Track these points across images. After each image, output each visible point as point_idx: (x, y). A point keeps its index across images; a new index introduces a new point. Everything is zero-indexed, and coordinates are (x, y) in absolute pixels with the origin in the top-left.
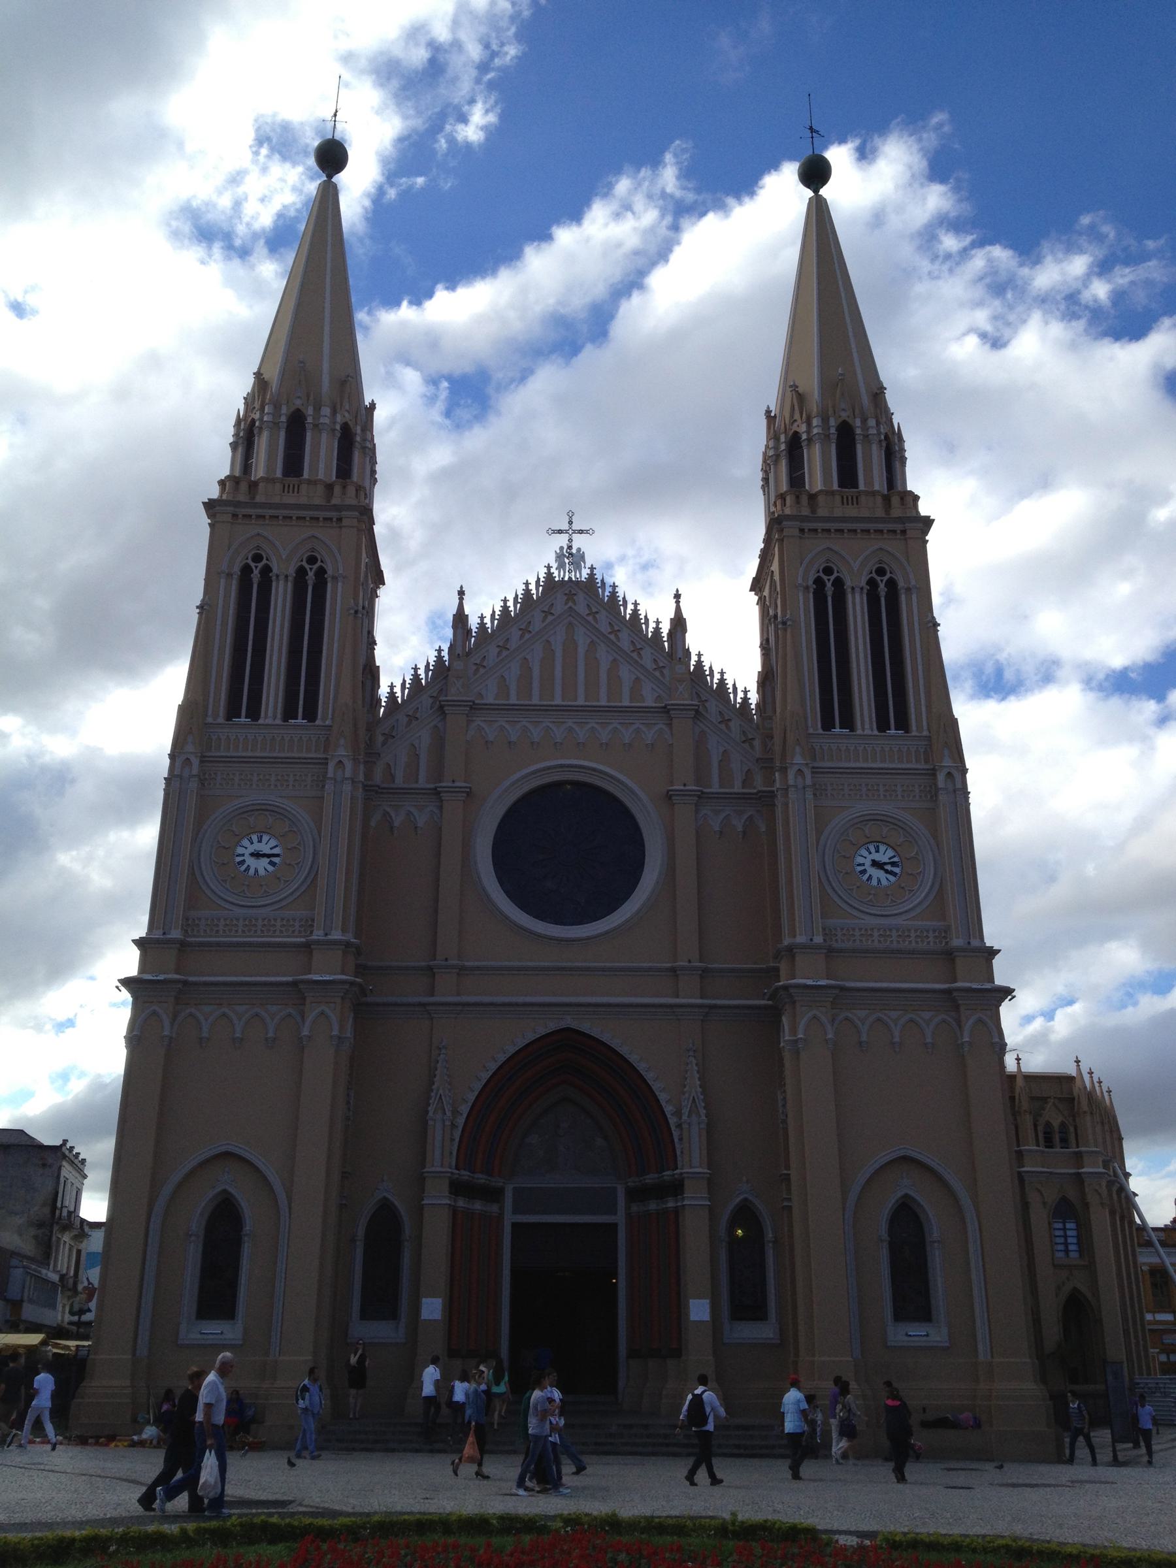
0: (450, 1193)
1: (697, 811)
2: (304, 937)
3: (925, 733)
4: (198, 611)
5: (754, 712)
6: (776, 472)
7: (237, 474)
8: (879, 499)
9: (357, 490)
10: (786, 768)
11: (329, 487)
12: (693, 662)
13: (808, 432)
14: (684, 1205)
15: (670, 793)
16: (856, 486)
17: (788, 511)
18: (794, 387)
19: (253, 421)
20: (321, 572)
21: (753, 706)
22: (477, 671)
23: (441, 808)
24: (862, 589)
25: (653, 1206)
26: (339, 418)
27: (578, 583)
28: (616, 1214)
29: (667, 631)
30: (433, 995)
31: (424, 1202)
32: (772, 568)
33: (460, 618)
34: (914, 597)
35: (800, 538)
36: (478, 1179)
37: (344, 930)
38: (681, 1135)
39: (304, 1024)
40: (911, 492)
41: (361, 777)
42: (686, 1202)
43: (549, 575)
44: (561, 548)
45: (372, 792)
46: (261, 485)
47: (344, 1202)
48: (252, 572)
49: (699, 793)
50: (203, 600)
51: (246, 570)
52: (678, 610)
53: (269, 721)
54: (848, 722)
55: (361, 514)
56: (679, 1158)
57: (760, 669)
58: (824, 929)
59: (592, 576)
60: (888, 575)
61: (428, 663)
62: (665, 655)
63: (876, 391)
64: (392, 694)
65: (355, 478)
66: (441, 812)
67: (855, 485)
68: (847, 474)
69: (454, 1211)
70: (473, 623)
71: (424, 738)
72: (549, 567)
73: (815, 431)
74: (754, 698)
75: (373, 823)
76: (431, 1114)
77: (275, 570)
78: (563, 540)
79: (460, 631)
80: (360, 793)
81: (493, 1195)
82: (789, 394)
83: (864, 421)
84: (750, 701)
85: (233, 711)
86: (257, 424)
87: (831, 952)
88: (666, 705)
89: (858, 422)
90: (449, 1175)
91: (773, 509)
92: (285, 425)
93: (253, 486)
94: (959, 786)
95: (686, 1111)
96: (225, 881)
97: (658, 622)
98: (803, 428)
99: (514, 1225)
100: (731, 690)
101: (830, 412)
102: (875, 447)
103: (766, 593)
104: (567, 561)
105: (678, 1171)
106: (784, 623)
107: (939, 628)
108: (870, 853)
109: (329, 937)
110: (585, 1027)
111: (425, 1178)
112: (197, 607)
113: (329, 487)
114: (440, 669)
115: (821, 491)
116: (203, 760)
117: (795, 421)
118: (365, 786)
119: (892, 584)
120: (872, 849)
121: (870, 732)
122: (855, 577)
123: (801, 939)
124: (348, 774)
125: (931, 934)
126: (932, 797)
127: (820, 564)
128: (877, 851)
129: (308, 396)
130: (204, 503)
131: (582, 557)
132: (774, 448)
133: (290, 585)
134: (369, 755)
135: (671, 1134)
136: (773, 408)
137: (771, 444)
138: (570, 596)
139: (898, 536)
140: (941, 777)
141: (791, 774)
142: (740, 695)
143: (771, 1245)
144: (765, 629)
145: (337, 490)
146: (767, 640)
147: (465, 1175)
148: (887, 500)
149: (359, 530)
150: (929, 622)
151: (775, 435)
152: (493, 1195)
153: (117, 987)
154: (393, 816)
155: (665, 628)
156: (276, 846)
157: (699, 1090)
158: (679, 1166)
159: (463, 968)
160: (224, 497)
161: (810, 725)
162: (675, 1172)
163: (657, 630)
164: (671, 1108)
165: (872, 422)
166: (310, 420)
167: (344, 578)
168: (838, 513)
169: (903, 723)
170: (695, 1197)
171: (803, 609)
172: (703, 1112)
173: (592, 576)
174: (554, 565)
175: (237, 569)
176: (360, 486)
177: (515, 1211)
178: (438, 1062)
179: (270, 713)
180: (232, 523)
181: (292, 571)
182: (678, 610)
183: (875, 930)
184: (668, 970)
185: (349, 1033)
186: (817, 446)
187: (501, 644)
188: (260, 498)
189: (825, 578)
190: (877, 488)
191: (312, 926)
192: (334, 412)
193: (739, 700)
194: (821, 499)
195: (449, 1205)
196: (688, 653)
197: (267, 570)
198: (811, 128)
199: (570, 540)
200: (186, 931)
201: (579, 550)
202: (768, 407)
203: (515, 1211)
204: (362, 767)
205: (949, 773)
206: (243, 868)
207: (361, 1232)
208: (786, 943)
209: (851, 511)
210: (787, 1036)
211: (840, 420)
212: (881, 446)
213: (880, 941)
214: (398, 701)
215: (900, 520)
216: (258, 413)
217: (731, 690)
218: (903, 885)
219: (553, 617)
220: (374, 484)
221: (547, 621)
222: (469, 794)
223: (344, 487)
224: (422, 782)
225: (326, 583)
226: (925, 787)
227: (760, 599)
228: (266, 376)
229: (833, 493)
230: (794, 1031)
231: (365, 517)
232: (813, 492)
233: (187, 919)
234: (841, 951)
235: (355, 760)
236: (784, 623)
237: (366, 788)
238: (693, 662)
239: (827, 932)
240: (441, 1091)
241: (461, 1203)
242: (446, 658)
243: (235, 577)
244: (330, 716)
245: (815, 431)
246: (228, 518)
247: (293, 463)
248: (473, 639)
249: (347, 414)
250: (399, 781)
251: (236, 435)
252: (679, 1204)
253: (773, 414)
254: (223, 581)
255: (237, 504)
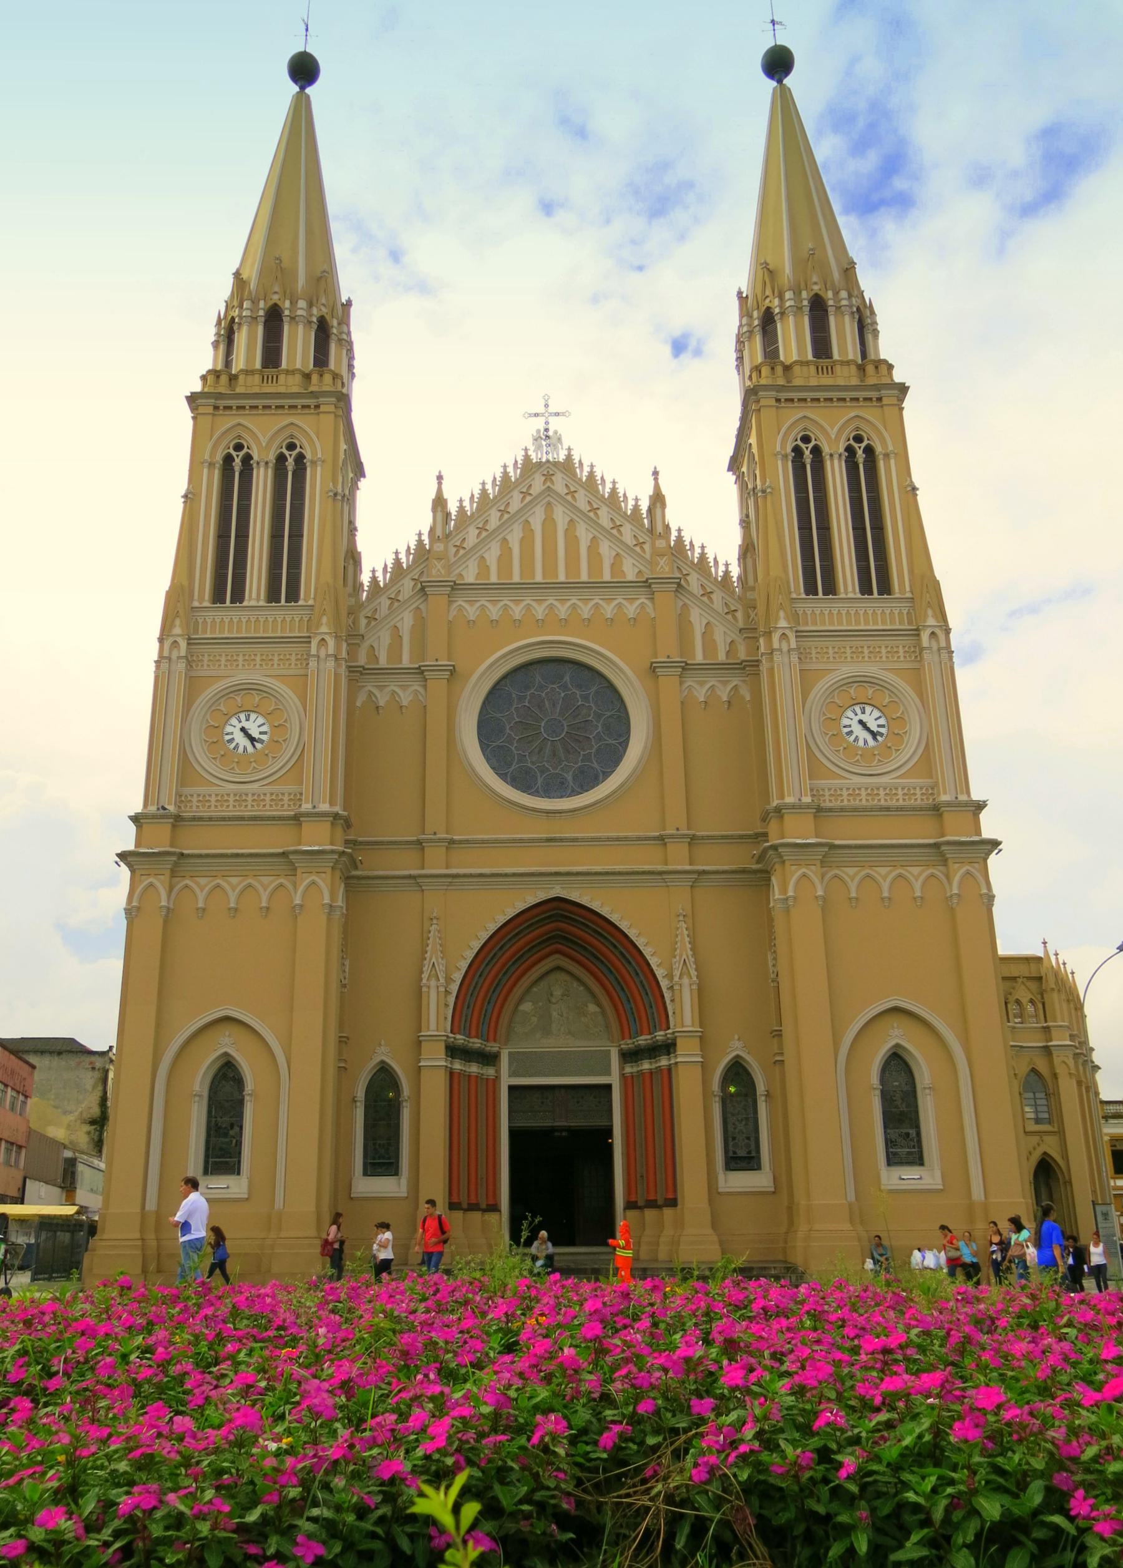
0: (447, 1056)
1: (681, 683)
2: (292, 810)
3: (908, 595)
4: (183, 500)
5: (736, 584)
6: (750, 349)
7: (219, 367)
8: (853, 368)
9: (334, 379)
10: (770, 633)
11: (307, 376)
12: (673, 538)
13: (781, 306)
14: (676, 1063)
15: (654, 665)
16: (831, 358)
17: (763, 382)
18: (765, 266)
19: (233, 319)
20: (300, 458)
21: (735, 579)
22: (457, 552)
23: (425, 687)
24: (840, 455)
25: (646, 1065)
26: (315, 311)
27: (556, 464)
28: (610, 1075)
29: (646, 508)
30: (423, 868)
31: (421, 1064)
32: (750, 441)
33: (439, 503)
34: (892, 462)
35: (777, 407)
36: (473, 1043)
37: (332, 803)
38: (673, 996)
39: (296, 893)
40: (885, 362)
41: (344, 655)
42: (679, 1060)
43: (527, 457)
44: (538, 431)
45: (357, 674)
46: (241, 378)
47: (343, 1065)
48: (234, 460)
49: (683, 664)
50: (188, 489)
51: (228, 459)
52: (657, 487)
53: (253, 603)
54: (830, 588)
55: (339, 400)
56: (671, 1018)
57: (740, 543)
58: (812, 790)
59: (569, 457)
60: (866, 442)
61: (409, 548)
62: (645, 531)
63: (846, 266)
64: (374, 579)
65: (332, 365)
66: (426, 690)
67: (829, 356)
68: (822, 346)
69: (451, 1073)
70: (453, 507)
71: (406, 621)
72: (526, 450)
73: (788, 304)
74: (735, 571)
75: (358, 704)
76: (424, 981)
77: (256, 457)
78: (539, 423)
79: (439, 515)
80: (343, 670)
81: (491, 1059)
82: (760, 273)
83: (836, 293)
84: (732, 574)
85: (218, 596)
86: (236, 320)
87: (819, 811)
88: (647, 579)
89: (830, 294)
90: (445, 1038)
91: (748, 383)
92: (263, 319)
93: (233, 378)
94: (943, 644)
95: (677, 973)
96: (233, 768)
97: (637, 500)
98: (776, 302)
99: (512, 1089)
100: (712, 564)
101: (803, 285)
102: (847, 318)
103: (744, 469)
104: (544, 443)
105: (670, 1031)
106: (764, 491)
107: (918, 492)
108: (856, 715)
109: (316, 810)
110: (574, 896)
111: (420, 1042)
112: (183, 497)
113: (307, 376)
114: (421, 553)
115: (795, 362)
116: (190, 642)
117: (767, 297)
118: (1101, 1329)
119: (869, 450)
120: (858, 711)
121: (850, 595)
122: (833, 446)
123: (789, 800)
124: (331, 651)
125: (918, 791)
126: (916, 657)
127: (797, 432)
128: (248, 720)
129: (285, 293)
130: (187, 397)
131: (559, 439)
132: (747, 324)
133: (270, 472)
134: (352, 637)
135: (663, 997)
136: (744, 289)
137: (744, 321)
138: (548, 477)
139: (875, 404)
140: (925, 636)
141: (776, 637)
142: (722, 568)
143: (763, 1098)
144: (745, 504)
145: (315, 378)
146: (747, 516)
147: (460, 1039)
148: (861, 368)
149: (336, 416)
150: (908, 485)
151: (748, 312)
152: (491, 1059)
153: (116, 863)
154: (378, 695)
155: (644, 506)
156: (264, 724)
157: (690, 953)
158: (671, 1026)
159: (452, 842)
160: (206, 390)
161: (793, 590)
162: (667, 1032)
163: (636, 508)
164: (662, 971)
165: (844, 294)
166: (287, 313)
167: (323, 462)
168: (813, 382)
169: (885, 588)
170: (687, 1053)
171: (783, 477)
172: (693, 973)
173: (569, 457)
174: (531, 448)
175: (219, 458)
176: (337, 375)
177: (512, 1074)
178: (430, 932)
179: (254, 595)
180: (214, 415)
181: (272, 457)
182: (657, 487)
183: (863, 789)
184: (654, 838)
185: (340, 902)
186: (791, 319)
187: (480, 526)
188: (239, 390)
189: (803, 446)
190: (851, 357)
191: (300, 800)
192: (310, 305)
193: (721, 574)
194: (797, 369)
195: (446, 1067)
196: (667, 528)
197: (247, 458)
198: (773, 22)
199: (547, 423)
200: (180, 807)
201: (556, 432)
202: (740, 289)
203: (512, 1074)
204: (344, 645)
205: (933, 633)
206: (232, 746)
207: (361, 1094)
208: (775, 803)
209: (827, 380)
210: (776, 894)
211: (812, 293)
212: (854, 318)
213: (867, 800)
214: (379, 586)
215: (877, 387)
216: (237, 311)
217: (712, 564)
218: (889, 745)
219: (531, 498)
220: (353, 379)
221: (525, 502)
222: (453, 672)
223: (321, 376)
224: (406, 662)
225: (305, 469)
226: (909, 647)
227: (738, 478)
228: (245, 276)
229: (807, 363)
230: (784, 890)
231: (342, 403)
232: (788, 363)
233: (181, 796)
234: (830, 810)
235: (337, 637)
236: (764, 491)
237: (351, 669)
238: (673, 538)
239: (815, 792)
240: (434, 960)
241: (458, 1065)
242: (427, 542)
243: (217, 465)
244: (312, 596)
245: (788, 304)
246: (210, 410)
247: (272, 356)
248: (453, 522)
249: (323, 309)
250: (383, 662)
251: (218, 334)
252: (672, 1062)
253: (744, 295)
254: (206, 471)
255: (219, 396)
